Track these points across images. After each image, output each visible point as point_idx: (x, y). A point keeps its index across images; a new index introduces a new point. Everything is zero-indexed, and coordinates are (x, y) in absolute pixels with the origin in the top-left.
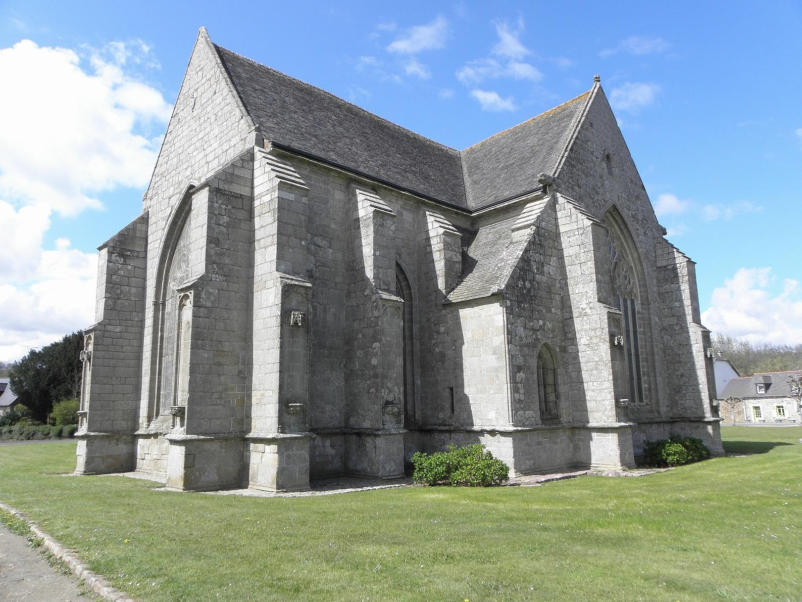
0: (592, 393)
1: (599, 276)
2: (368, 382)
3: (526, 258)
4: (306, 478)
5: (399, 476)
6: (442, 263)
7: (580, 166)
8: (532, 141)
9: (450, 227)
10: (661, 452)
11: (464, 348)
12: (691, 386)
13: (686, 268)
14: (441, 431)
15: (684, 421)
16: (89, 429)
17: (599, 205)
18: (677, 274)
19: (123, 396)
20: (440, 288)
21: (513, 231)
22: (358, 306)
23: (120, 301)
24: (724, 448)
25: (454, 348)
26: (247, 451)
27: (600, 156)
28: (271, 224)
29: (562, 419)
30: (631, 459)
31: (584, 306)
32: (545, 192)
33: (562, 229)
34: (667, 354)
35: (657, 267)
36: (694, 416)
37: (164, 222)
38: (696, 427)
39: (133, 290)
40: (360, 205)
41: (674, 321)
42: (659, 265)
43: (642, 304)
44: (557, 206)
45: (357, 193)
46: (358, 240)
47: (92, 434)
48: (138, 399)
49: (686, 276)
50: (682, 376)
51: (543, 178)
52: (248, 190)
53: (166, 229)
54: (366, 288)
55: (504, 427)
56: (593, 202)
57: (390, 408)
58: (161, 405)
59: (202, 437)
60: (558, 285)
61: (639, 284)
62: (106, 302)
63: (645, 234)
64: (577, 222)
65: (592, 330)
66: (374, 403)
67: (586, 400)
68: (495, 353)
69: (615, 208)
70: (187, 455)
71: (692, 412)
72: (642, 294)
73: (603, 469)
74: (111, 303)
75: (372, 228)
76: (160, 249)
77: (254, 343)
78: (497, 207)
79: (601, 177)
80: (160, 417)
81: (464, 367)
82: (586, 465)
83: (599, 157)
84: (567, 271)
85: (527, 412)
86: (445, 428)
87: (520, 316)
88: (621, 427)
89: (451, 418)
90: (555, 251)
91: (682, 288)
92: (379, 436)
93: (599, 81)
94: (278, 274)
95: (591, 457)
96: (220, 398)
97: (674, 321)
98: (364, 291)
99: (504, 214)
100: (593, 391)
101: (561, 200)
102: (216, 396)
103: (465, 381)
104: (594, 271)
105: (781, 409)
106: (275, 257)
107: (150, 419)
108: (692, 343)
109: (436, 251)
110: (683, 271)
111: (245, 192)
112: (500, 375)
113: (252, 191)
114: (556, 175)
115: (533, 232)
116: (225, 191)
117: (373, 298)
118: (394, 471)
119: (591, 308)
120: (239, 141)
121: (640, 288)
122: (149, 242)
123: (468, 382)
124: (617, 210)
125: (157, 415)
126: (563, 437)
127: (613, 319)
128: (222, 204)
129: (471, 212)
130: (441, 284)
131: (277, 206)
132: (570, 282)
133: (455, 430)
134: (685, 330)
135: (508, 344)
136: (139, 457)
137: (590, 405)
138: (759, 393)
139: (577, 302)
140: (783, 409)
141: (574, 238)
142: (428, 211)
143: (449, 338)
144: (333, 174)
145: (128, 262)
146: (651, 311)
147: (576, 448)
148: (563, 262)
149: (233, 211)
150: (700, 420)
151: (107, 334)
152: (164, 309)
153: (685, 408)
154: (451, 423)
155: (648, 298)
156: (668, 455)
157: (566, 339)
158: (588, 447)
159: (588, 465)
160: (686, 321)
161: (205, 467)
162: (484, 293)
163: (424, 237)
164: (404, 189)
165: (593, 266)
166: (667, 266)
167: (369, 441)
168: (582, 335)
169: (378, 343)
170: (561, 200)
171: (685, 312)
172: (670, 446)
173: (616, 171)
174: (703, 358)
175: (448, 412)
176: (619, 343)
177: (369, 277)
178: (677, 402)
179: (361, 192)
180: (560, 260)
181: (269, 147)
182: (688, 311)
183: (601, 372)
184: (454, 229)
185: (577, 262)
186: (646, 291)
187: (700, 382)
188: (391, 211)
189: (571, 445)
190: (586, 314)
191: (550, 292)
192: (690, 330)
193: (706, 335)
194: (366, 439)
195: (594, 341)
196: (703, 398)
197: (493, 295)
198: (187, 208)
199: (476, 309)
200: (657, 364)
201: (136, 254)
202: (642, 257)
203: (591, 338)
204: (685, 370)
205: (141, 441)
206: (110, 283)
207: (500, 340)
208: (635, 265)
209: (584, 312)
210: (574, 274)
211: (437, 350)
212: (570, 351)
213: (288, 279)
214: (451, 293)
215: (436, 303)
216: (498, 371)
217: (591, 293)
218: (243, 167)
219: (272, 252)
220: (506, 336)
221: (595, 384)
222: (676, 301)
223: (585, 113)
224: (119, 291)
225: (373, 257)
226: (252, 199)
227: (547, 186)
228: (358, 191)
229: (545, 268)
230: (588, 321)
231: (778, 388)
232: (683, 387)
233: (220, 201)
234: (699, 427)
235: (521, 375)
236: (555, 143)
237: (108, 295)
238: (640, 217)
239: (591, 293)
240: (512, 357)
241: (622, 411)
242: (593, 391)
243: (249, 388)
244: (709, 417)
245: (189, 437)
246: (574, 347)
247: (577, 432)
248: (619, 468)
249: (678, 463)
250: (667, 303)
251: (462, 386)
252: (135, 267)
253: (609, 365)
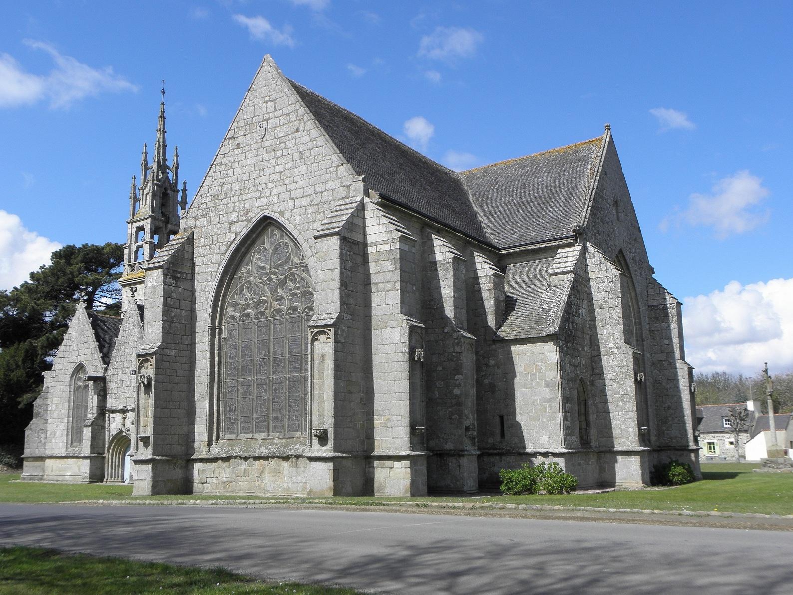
1: (624, 320)
3: (569, 303)
5: (476, 491)
6: (492, 302)
9: (493, 267)
11: (516, 380)
12: (676, 417)
14: (492, 454)
15: (670, 450)
16: (154, 453)
18: (667, 313)
19: (178, 420)
20: (490, 325)
21: (551, 275)
22: (437, 341)
24: (702, 475)
26: (370, 467)
27: (611, 203)
28: (392, 271)
30: (648, 480)
31: (612, 346)
32: (576, 241)
33: (592, 275)
34: (656, 387)
36: (679, 444)
37: (224, 248)
38: (681, 455)
39: (184, 313)
40: (437, 249)
41: (663, 357)
42: (650, 303)
43: (637, 341)
44: (587, 253)
46: (435, 281)
47: (157, 458)
49: (675, 316)
50: (669, 408)
51: (577, 228)
52: (362, 236)
53: (227, 254)
54: (446, 325)
56: (608, 248)
57: (470, 432)
58: (221, 430)
60: (588, 326)
62: (163, 325)
63: (641, 274)
64: (606, 270)
66: (457, 428)
68: (548, 386)
69: (621, 251)
70: (336, 470)
71: (677, 441)
73: (627, 486)
76: (218, 274)
78: (528, 248)
79: (613, 223)
80: (221, 442)
82: (612, 484)
84: (596, 314)
89: (501, 442)
90: (585, 295)
91: (672, 327)
92: (463, 456)
93: (609, 129)
94: (405, 317)
95: (615, 477)
96: (351, 422)
97: (663, 357)
98: (444, 328)
99: (533, 255)
100: (618, 420)
101: (591, 249)
104: (621, 315)
106: (399, 301)
107: (210, 443)
108: (679, 378)
110: (672, 312)
111: (359, 239)
112: (553, 405)
113: (364, 238)
114: (585, 225)
115: (572, 279)
116: (349, 238)
117: (455, 335)
118: (473, 486)
120: (339, 186)
121: (636, 326)
122: (196, 264)
123: (520, 410)
124: (622, 253)
125: (218, 439)
126: (593, 459)
127: (638, 361)
128: (347, 250)
129: (499, 250)
130: (491, 321)
131: (398, 256)
134: (673, 366)
136: (196, 480)
137: (615, 432)
138: (725, 426)
139: (605, 342)
140: (714, 446)
141: (603, 285)
143: (499, 371)
144: (450, 235)
145: (180, 284)
146: (644, 348)
147: (602, 470)
150: (685, 449)
152: (220, 334)
153: (671, 438)
154: (502, 446)
156: (674, 476)
159: (612, 484)
160: (674, 358)
161: (344, 480)
163: (472, 275)
165: (620, 311)
166: (658, 306)
168: (609, 371)
169: (460, 376)
170: (591, 249)
173: (622, 215)
174: (688, 392)
175: (498, 438)
176: (641, 379)
178: (663, 432)
180: (589, 303)
181: (377, 198)
182: (677, 348)
183: (625, 404)
186: (641, 329)
187: (685, 413)
188: (461, 256)
189: (598, 467)
190: (613, 353)
192: (678, 366)
193: (690, 369)
194: (448, 459)
196: (687, 428)
199: (529, 346)
202: (639, 297)
203: (617, 374)
205: (197, 466)
206: (166, 306)
208: (632, 304)
209: (611, 351)
211: (486, 381)
212: (597, 384)
213: (412, 321)
214: (500, 330)
215: (485, 338)
216: (551, 401)
217: (618, 334)
218: (358, 216)
221: (620, 414)
223: (602, 163)
225: (453, 299)
226: (365, 245)
227: (579, 235)
228: (434, 237)
230: (615, 359)
231: (710, 423)
233: (346, 249)
234: (683, 454)
235: (568, 405)
237: (165, 318)
238: (637, 259)
239: (618, 334)
240: (563, 390)
241: (643, 438)
242: (618, 420)
244: (692, 445)
245: (337, 454)
246: (601, 381)
249: (681, 483)
252: (185, 289)
253: (633, 397)
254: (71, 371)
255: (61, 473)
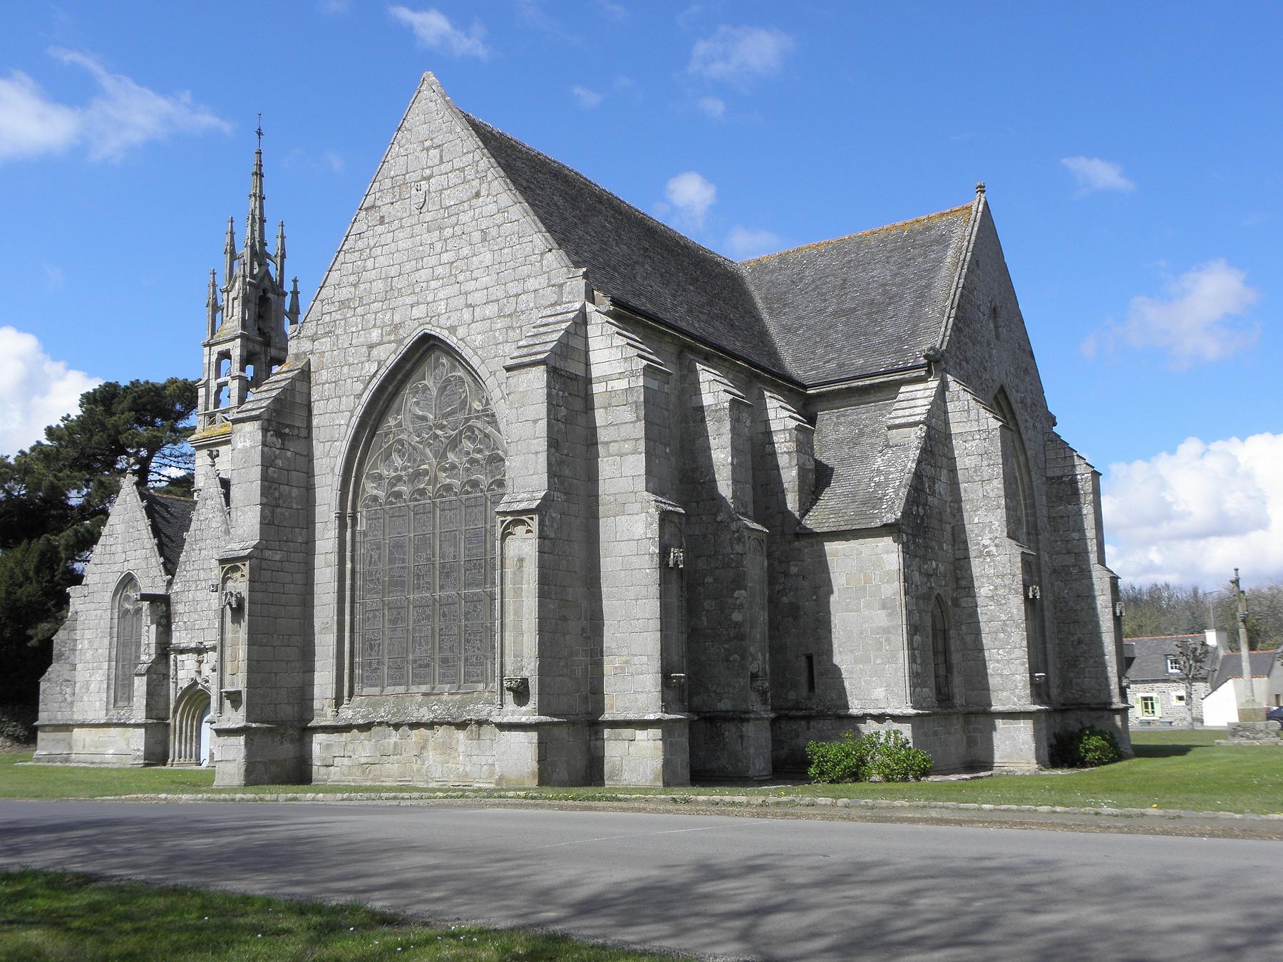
0: (997, 665)
2: (726, 646)
4: (686, 774)
6: (794, 472)
7: (967, 330)
8: (879, 273)
10: (1079, 748)
11: (833, 598)
12: (1092, 657)
13: (1091, 483)
14: (794, 718)
15: (1080, 709)
17: (987, 387)
18: (1077, 489)
21: (890, 428)
22: (705, 536)
23: (279, 510)
25: (815, 597)
26: (596, 740)
28: (631, 422)
29: (955, 701)
30: (1046, 758)
31: (987, 542)
33: (954, 429)
35: (1047, 478)
39: (295, 492)
41: (1069, 560)
42: (1050, 474)
43: (1029, 534)
44: (947, 393)
45: (698, 368)
47: (254, 725)
48: (308, 666)
50: (1080, 642)
51: (931, 353)
52: (582, 366)
55: (900, 710)
59: (556, 720)
60: (948, 510)
61: (1025, 504)
64: (978, 420)
65: (998, 576)
67: (987, 674)
69: (1002, 390)
70: (541, 743)
72: (1029, 518)
73: (1012, 769)
74: (269, 514)
75: (727, 426)
76: (350, 429)
77: (604, 590)
80: (356, 699)
81: (833, 626)
82: (988, 765)
83: (986, 313)
85: (924, 690)
86: (800, 713)
87: (916, 556)
88: (1039, 711)
89: (809, 698)
91: (1085, 512)
92: (747, 720)
93: (983, 192)
94: (653, 497)
97: (1069, 560)
98: (716, 515)
99: (860, 396)
100: (998, 661)
101: (954, 386)
102: (562, 663)
103: (835, 646)
104: (1002, 493)
105: (1149, 702)
106: (643, 471)
107: (338, 702)
108: (1096, 593)
109: (782, 453)
110: (1085, 486)
111: (579, 370)
112: (892, 638)
114: (944, 348)
116: (562, 370)
119: (996, 546)
122: (315, 412)
125: (351, 694)
129: (806, 387)
130: (792, 503)
131: (642, 399)
132: (966, 507)
133: (818, 716)
134: (1086, 574)
135: (905, 595)
137: (993, 681)
138: (1170, 671)
139: (977, 535)
140: (1152, 704)
142: (767, 391)
143: (806, 583)
144: (667, 339)
145: (289, 445)
146: (1040, 545)
147: (971, 742)
148: (956, 476)
149: (569, 398)
151: (265, 564)
153: (1083, 691)
154: (809, 705)
155: (1036, 525)
156: (1087, 751)
157: (958, 587)
158: (990, 740)
162: (864, 521)
163: (762, 428)
164: (739, 358)
165: (1001, 486)
166: (1062, 477)
167: (730, 731)
168: (983, 583)
169: (743, 592)
170: (954, 386)
171: (1087, 548)
172: (1089, 739)
173: (1003, 331)
174: (1110, 616)
175: (804, 691)
177: (724, 495)
178: (1071, 681)
179: (702, 367)
181: (607, 305)
182: (1092, 546)
183: (1010, 636)
184: (801, 418)
185: (977, 479)
186: (1034, 515)
187: (1106, 651)
189: (965, 738)
191: (941, 521)
193: (1114, 580)
194: (723, 726)
195: (1001, 592)
196: (1110, 675)
197: (885, 525)
198: (407, 368)
199: (853, 544)
200: (1047, 624)
201: (296, 432)
202: (1031, 463)
203: (996, 588)
204: (1083, 634)
205: (318, 740)
207: (894, 589)
210: (972, 496)
211: (785, 600)
213: (665, 503)
216: (890, 632)
217: (997, 524)
218: (576, 334)
219: (636, 464)
220: (902, 584)
221: (1001, 652)
222: (1074, 531)
224: (277, 494)
225: (730, 467)
226: (588, 381)
227: (935, 363)
229: (937, 486)
232: (1081, 659)
233: (557, 387)
235: (917, 638)
236: (926, 287)
238: (1029, 402)
239: (997, 524)
240: (909, 614)
241: (1039, 690)
242: (998, 661)
243: (599, 653)
244: (1117, 703)
245: (544, 718)
247: (973, 719)
248: (1034, 766)
249: (1100, 762)
250: (1061, 533)
251: (830, 652)
252: (296, 453)
254: (113, 587)
255: (99, 750)
